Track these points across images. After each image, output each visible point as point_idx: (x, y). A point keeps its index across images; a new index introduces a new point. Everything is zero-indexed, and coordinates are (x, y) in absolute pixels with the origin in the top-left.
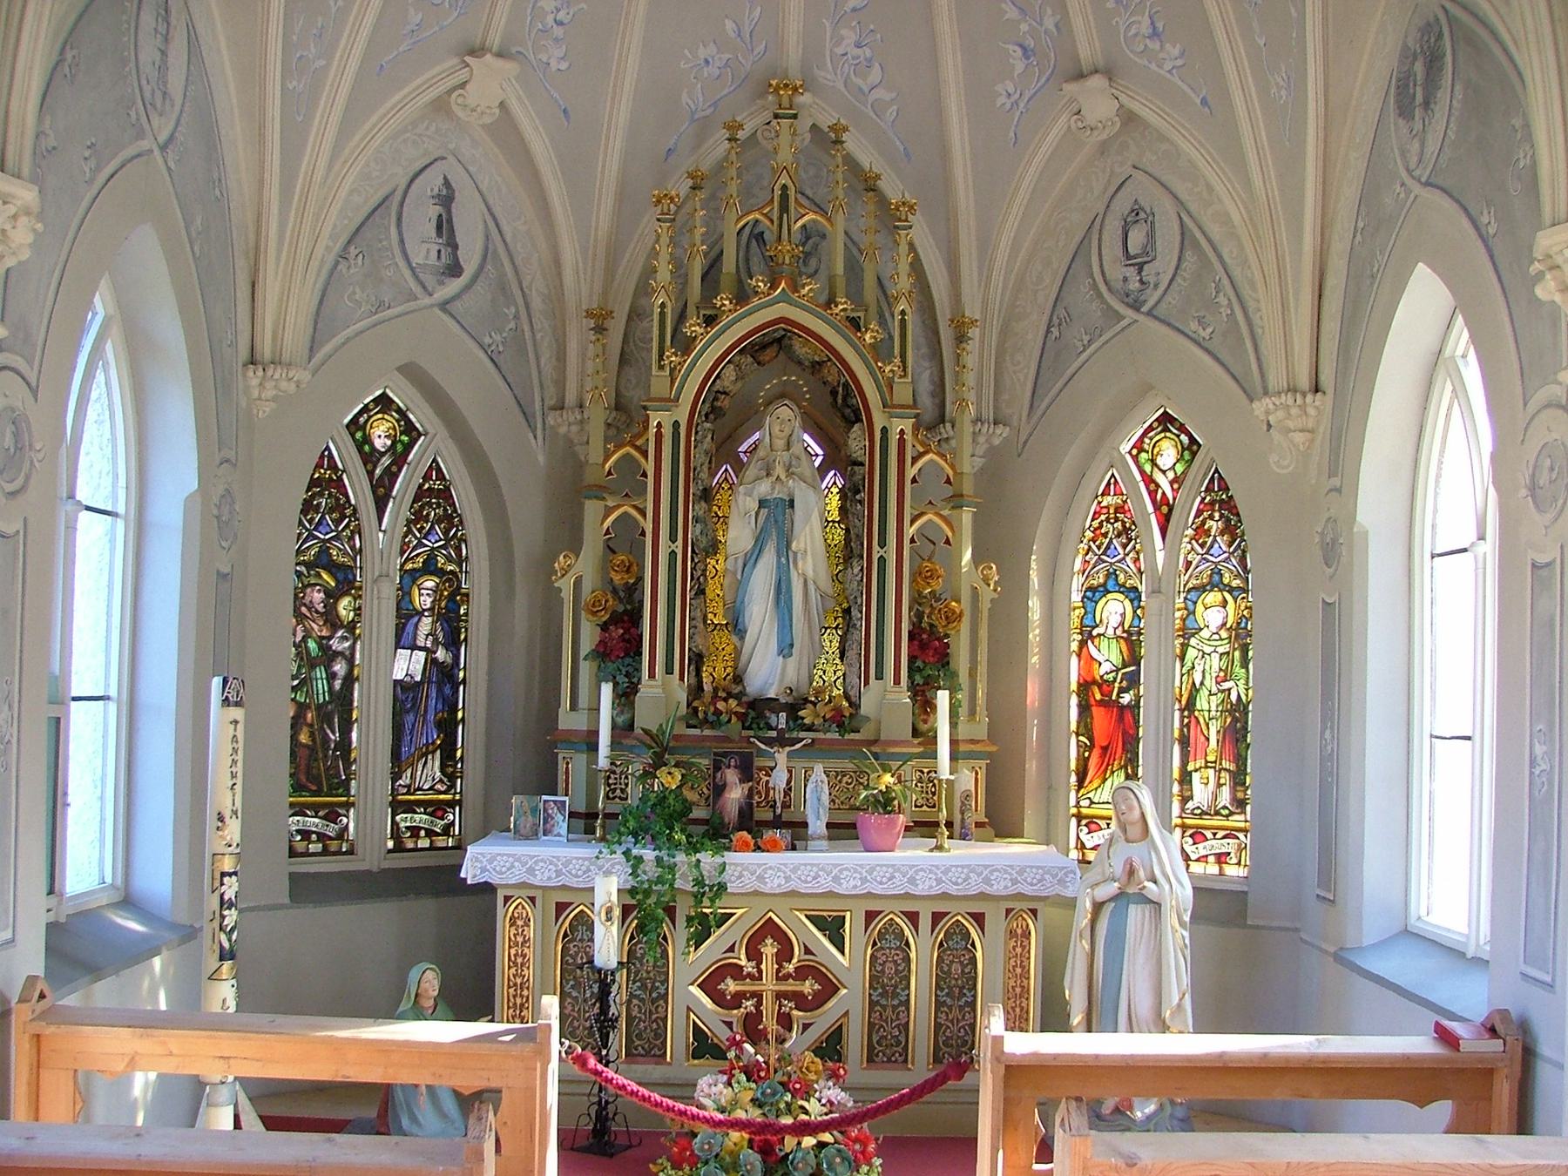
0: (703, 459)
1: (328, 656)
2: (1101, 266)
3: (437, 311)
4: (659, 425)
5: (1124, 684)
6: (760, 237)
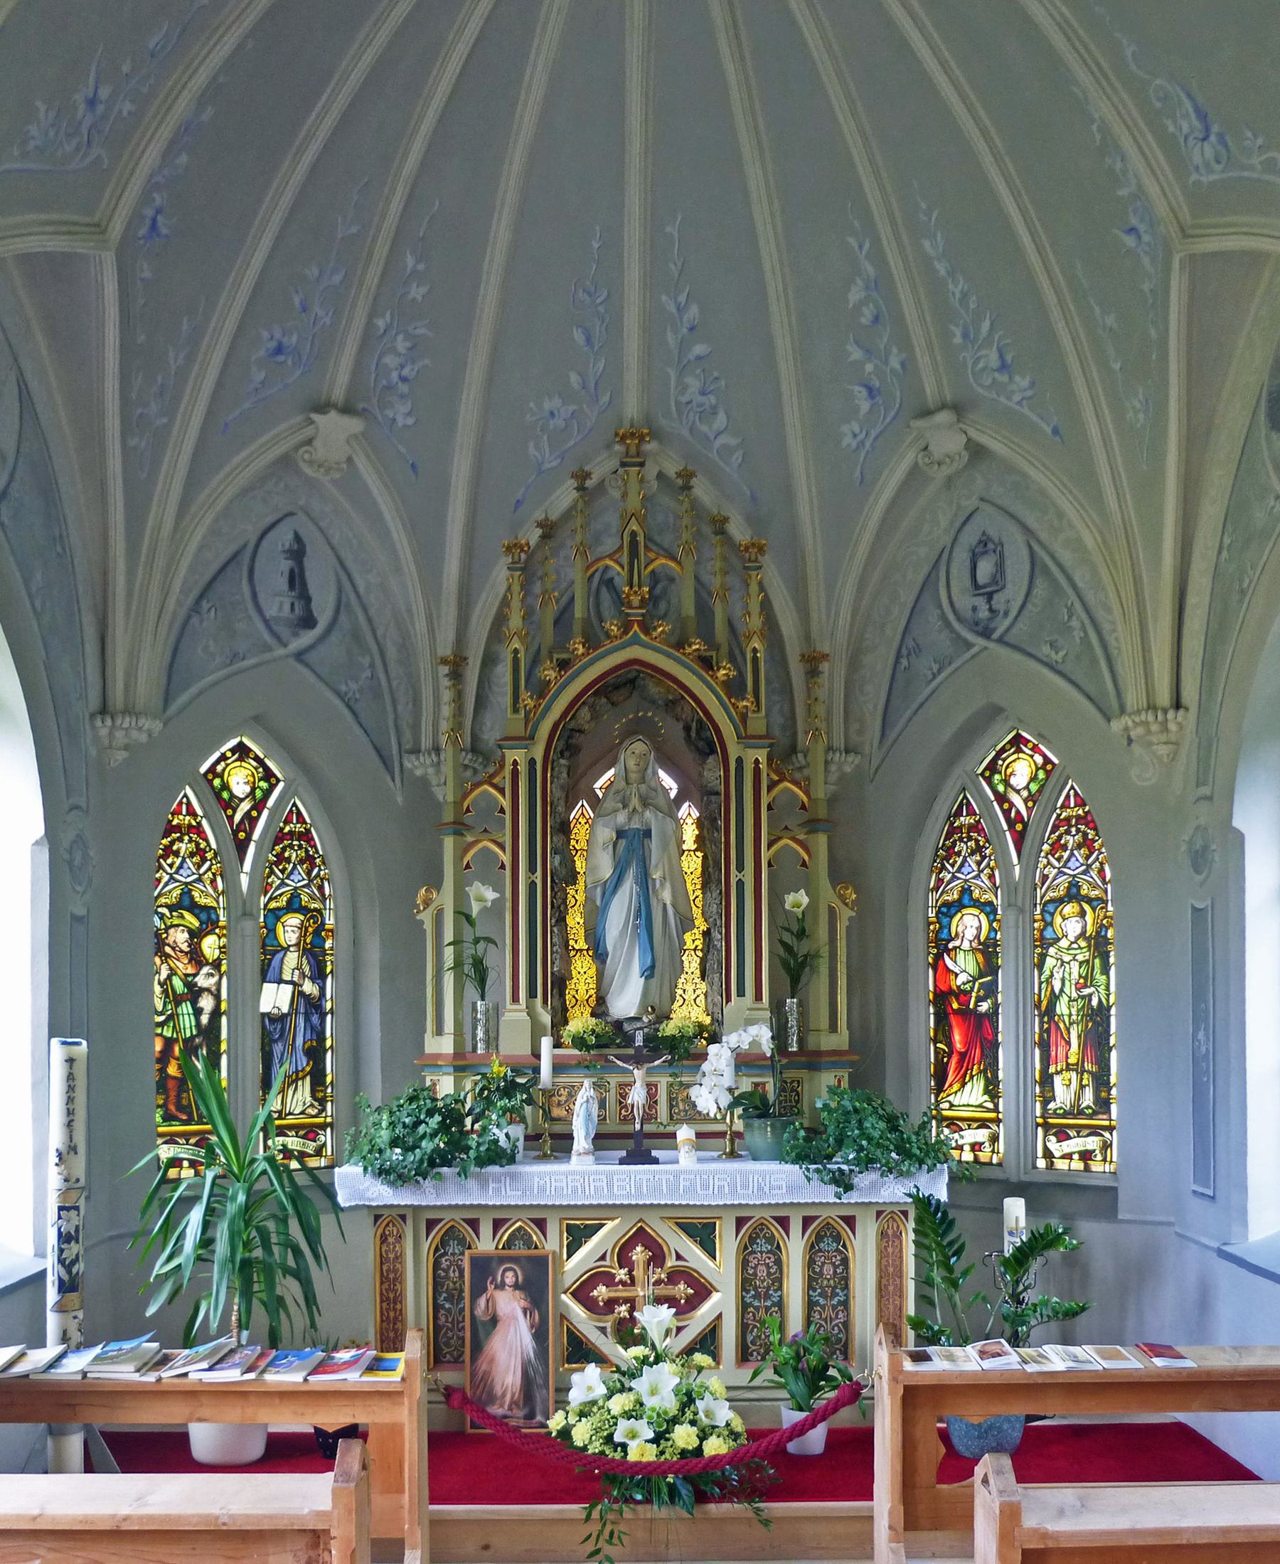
0: (558, 793)
1: (194, 993)
2: (950, 597)
3: (292, 662)
4: (515, 763)
5: (982, 993)
6: (609, 583)
